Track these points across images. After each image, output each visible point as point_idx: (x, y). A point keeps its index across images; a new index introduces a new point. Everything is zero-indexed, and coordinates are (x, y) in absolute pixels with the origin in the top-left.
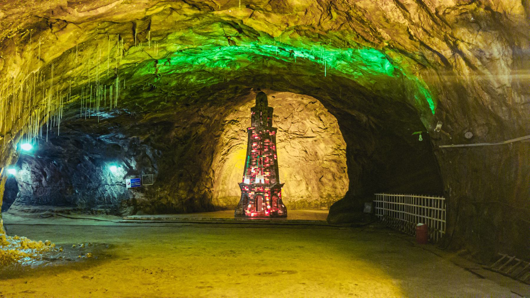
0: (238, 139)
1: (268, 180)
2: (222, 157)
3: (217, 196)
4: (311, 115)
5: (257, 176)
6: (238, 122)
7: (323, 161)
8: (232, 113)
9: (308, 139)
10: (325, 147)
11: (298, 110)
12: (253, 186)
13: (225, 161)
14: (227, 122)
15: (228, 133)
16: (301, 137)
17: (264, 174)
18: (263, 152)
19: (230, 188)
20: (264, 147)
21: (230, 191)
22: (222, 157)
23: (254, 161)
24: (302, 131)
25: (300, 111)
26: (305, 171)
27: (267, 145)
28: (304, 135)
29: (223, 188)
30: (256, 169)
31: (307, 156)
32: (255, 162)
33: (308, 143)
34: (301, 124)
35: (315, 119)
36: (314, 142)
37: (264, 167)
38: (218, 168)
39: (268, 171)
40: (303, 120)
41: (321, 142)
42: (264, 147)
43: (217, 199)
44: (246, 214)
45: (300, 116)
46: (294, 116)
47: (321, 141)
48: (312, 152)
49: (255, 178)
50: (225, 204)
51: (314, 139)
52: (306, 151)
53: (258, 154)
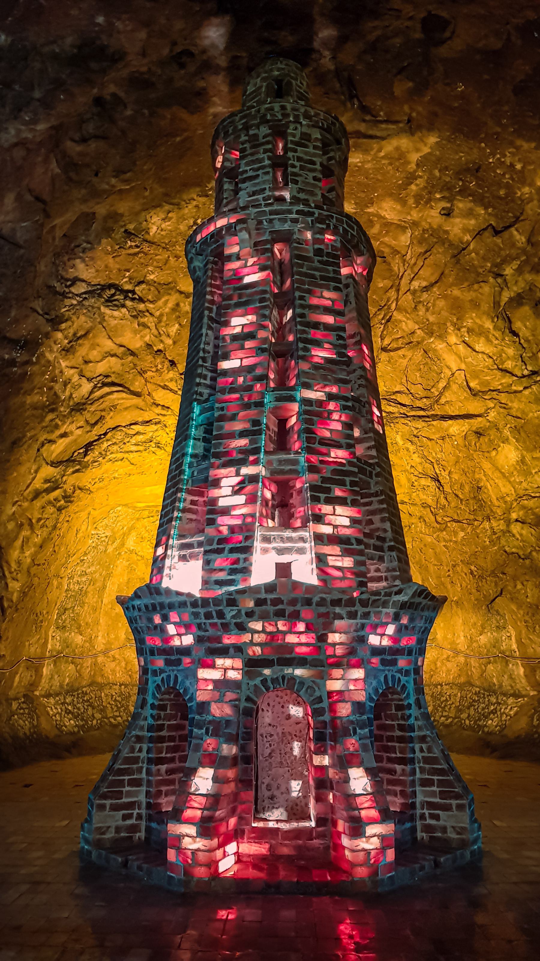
0: (138, 395)
1: (348, 562)
2: (48, 471)
3: (33, 685)
4: (475, 304)
5: (258, 534)
6: (141, 300)
7: (508, 522)
8: (106, 244)
9: (446, 424)
10: (523, 461)
11: (416, 284)
12: (230, 613)
13: (68, 498)
14: (81, 288)
15: (86, 344)
16: (420, 417)
17: (319, 519)
18: (304, 366)
19: (100, 642)
20: (311, 334)
21: (100, 659)
22: (48, 471)
23: (238, 426)
24: (422, 393)
25: (426, 289)
26: (431, 568)
27: (327, 327)
28: (431, 407)
29: (66, 644)
30: (253, 479)
31: (443, 501)
32: (243, 434)
33: (447, 446)
34: (419, 355)
35: (488, 325)
36: (473, 438)
37: (312, 469)
38: (26, 532)
39: (342, 502)
40: (431, 334)
41: (506, 441)
42: (311, 334)
43: (29, 698)
44: (171, 855)
45: (422, 311)
46: (397, 316)
47: (507, 432)
48: (462, 486)
49: (248, 550)
50: (70, 723)
51: (477, 423)
52: (436, 479)
53: (264, 378)
